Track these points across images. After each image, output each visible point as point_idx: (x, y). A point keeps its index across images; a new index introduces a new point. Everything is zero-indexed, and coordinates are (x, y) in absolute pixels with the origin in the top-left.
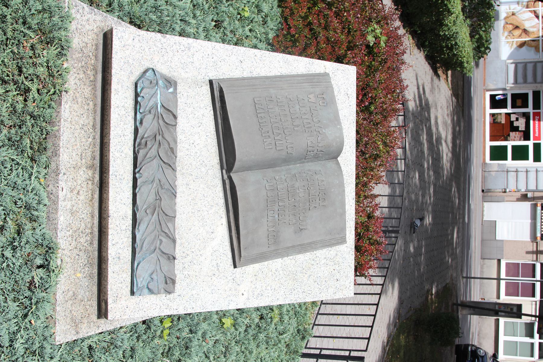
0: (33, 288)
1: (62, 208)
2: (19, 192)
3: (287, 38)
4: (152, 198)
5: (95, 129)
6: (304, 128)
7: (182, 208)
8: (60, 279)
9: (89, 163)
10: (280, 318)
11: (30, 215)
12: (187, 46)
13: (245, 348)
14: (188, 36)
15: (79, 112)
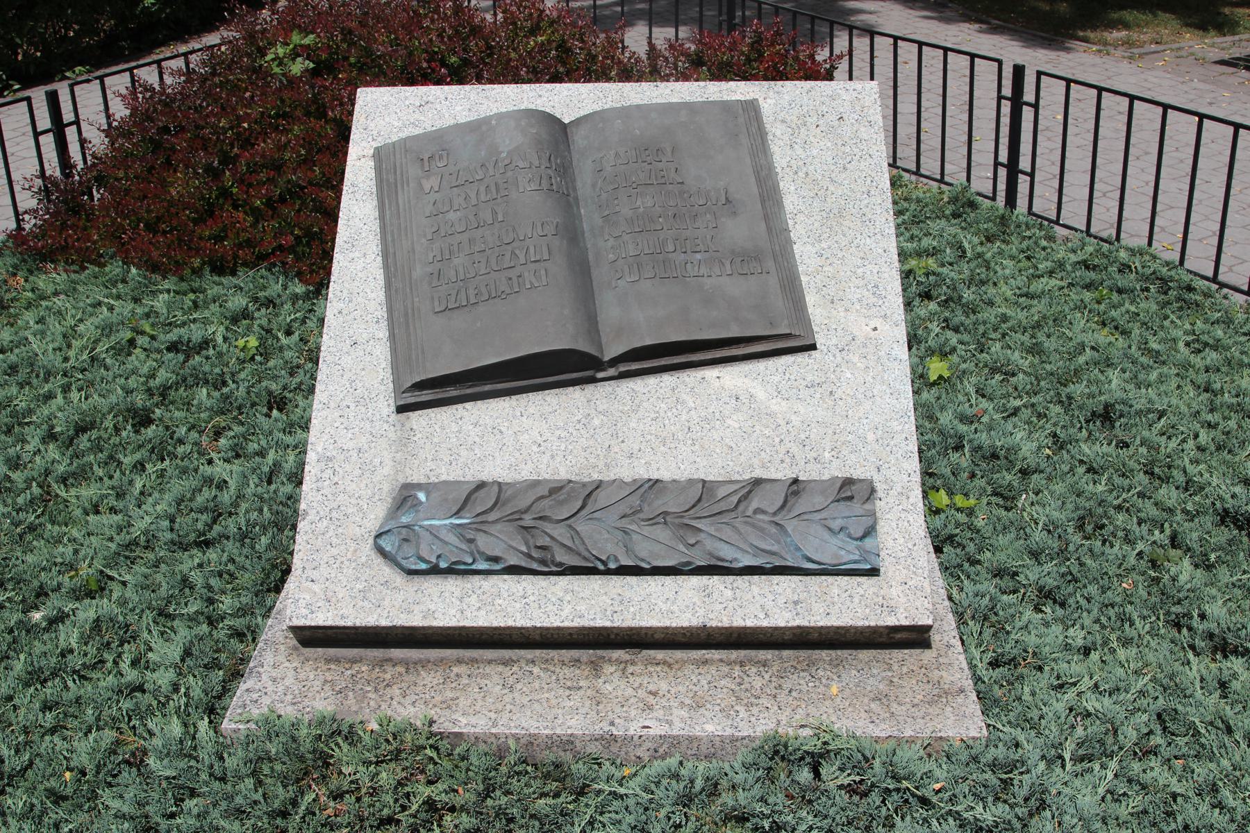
0: (863, 787)
1: (687, 728)
2: (653, 820)
3: (304, 254)
4: (661, 533)
5: (513, 661)
6: (499, 200)
7: (682, 467)
8: (844, 730)
9: (586, 673)
10: (927, 256)
11: (703, 796)
12: (323, 464)
13: (995, 330)
14: (302, 465)
15: (476, 696)
